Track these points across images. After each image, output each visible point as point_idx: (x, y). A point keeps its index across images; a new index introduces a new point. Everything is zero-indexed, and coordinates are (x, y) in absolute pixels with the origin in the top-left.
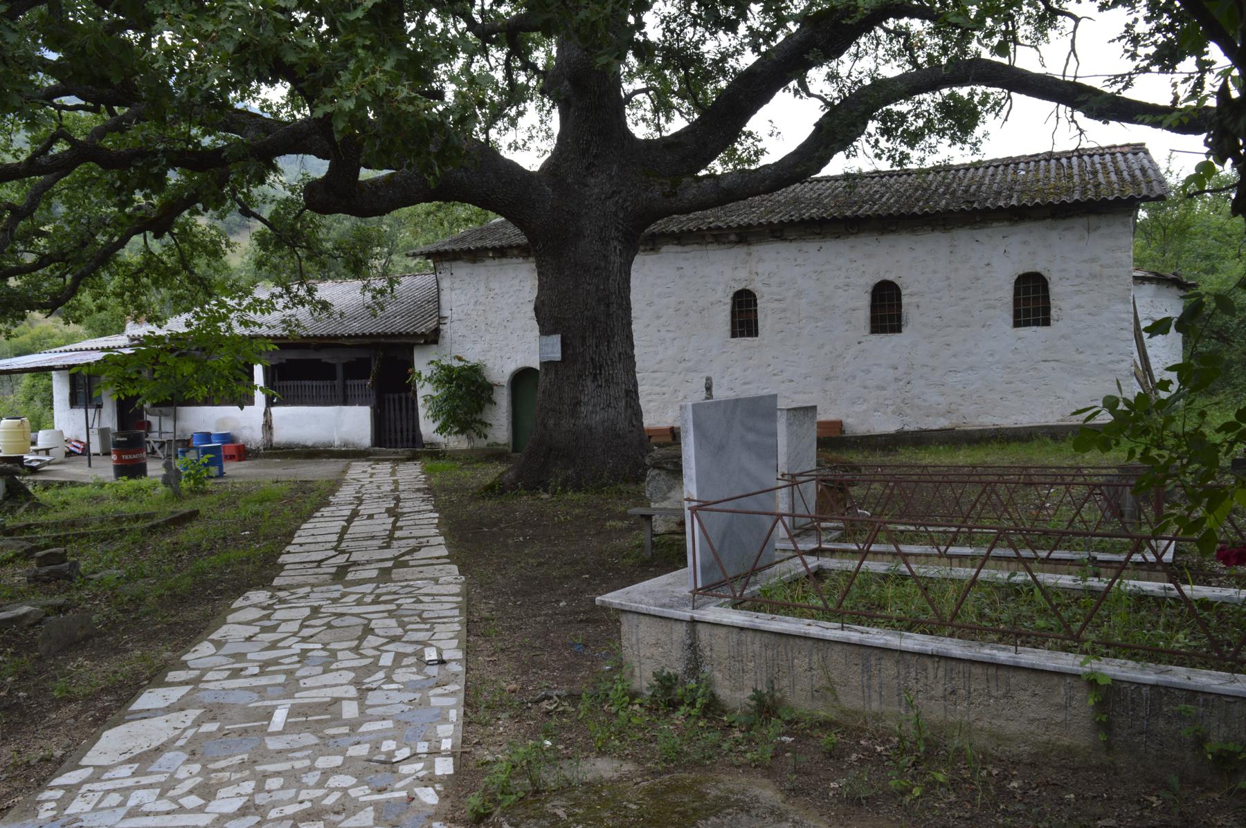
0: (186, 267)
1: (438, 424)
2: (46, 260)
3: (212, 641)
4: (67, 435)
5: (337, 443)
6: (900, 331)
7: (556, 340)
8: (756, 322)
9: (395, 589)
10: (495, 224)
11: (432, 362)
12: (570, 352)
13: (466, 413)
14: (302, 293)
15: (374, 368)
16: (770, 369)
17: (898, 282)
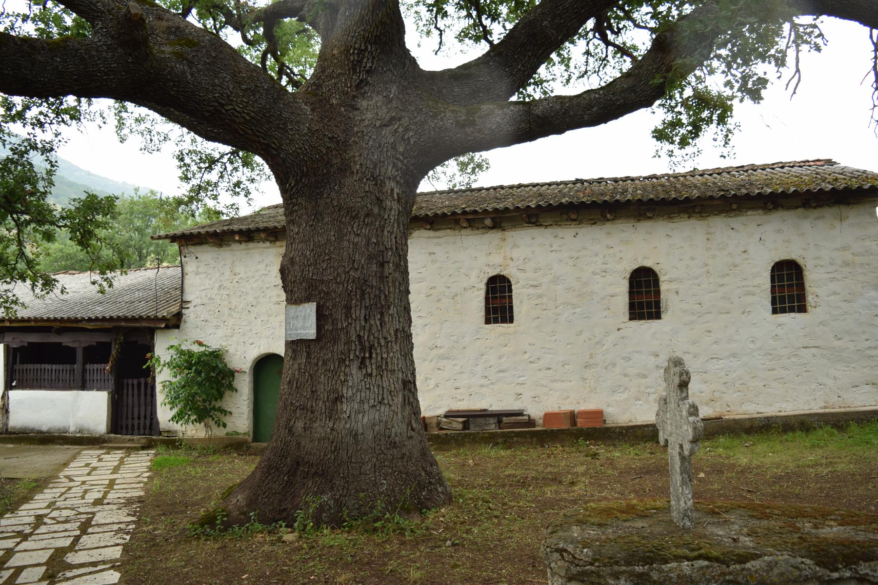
1: (175, 411)
5: (72, 429)
6: (657, 316)
7: (310, 309)
8: (511, 308)
11: (172, 347)
12: (328, 327)
15: (114, 352)
16: (526, 356)
17: (656, 269)
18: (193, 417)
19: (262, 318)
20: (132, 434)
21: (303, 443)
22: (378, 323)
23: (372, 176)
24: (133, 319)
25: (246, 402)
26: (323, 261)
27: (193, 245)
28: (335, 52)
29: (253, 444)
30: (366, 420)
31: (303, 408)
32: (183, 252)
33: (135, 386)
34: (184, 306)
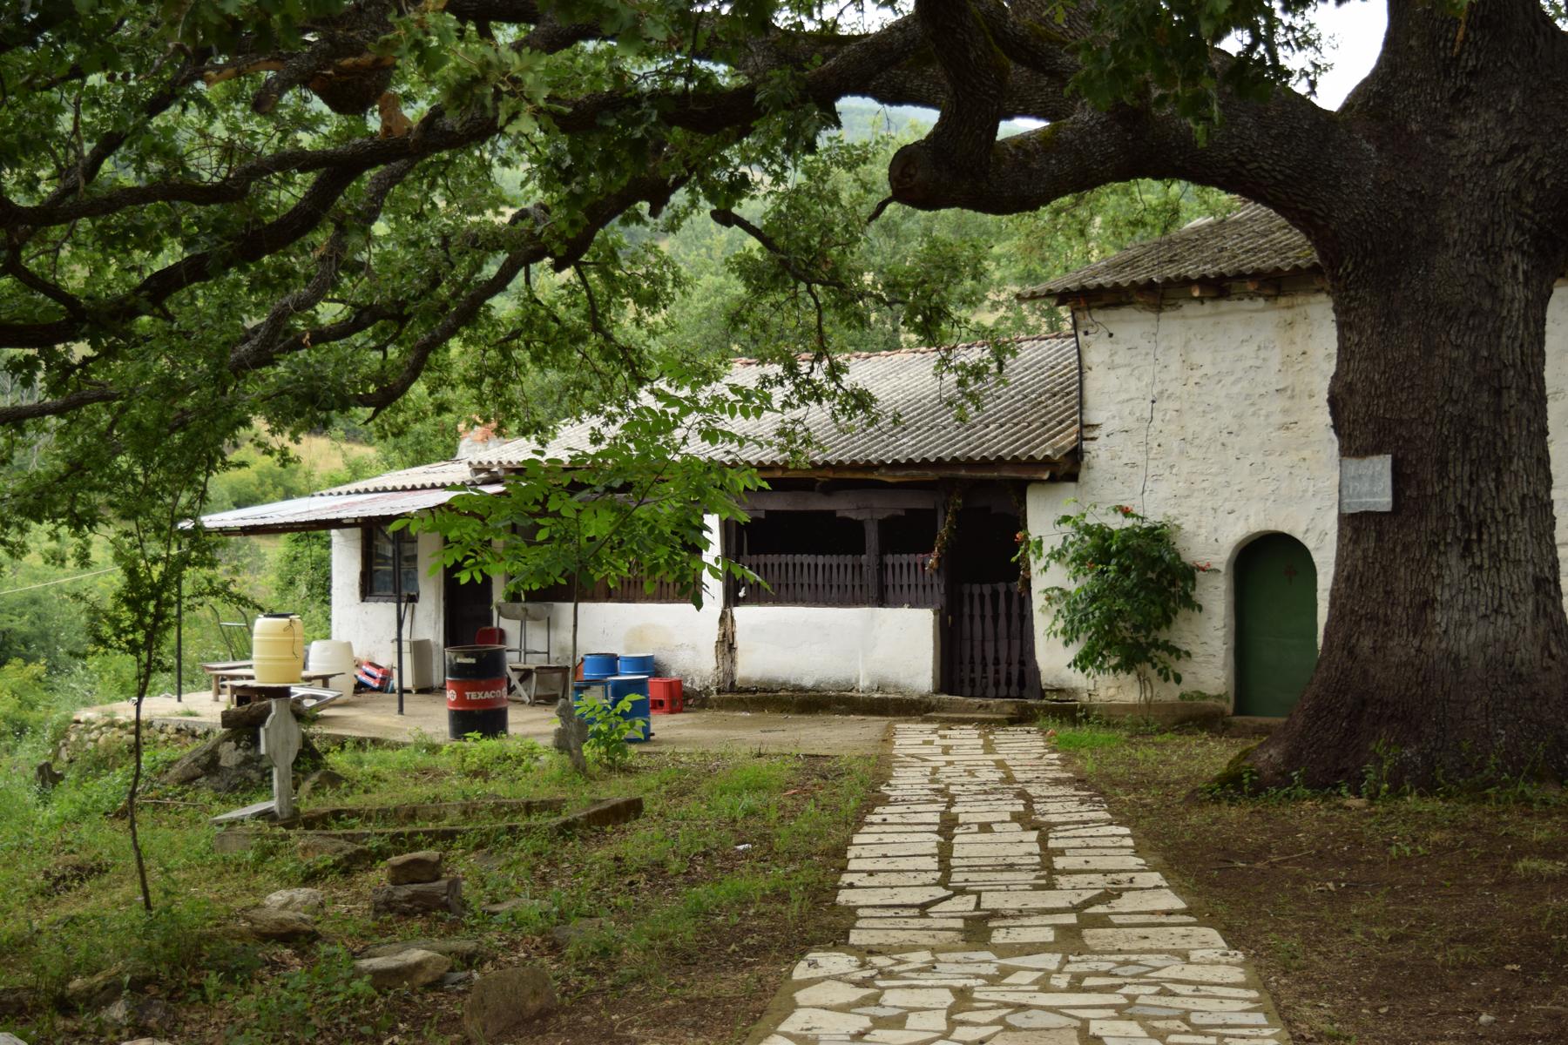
0: (597, 327)
1: (1075, 649)
2: (366, 316)
3: (788, 1035)
4: (360, 652)
5: (863, 683)
7: (1380, 468)
9: (1105, 967)
10: (1197, 230)
11: (1066, 519)
12: (1412, 492)
13: (1136, 628)
14: (819, 375)
15: (943, 531)
18: (1114, 661)
19: (1251, 458)
20: (984, 695)
21: (1372, 671)
22: (1492, 485)
23: (1480, 248)
24: (985, 463)
25: (1221, 633)
26: (1402, 390)
27: (1100, 308)
28: (1413, 42)
29: (1236, 719)
30: (1472, 637)
31: (1372, 617)
32: (1082, 322)
33: (987, 599)
34: (1086, 435)
